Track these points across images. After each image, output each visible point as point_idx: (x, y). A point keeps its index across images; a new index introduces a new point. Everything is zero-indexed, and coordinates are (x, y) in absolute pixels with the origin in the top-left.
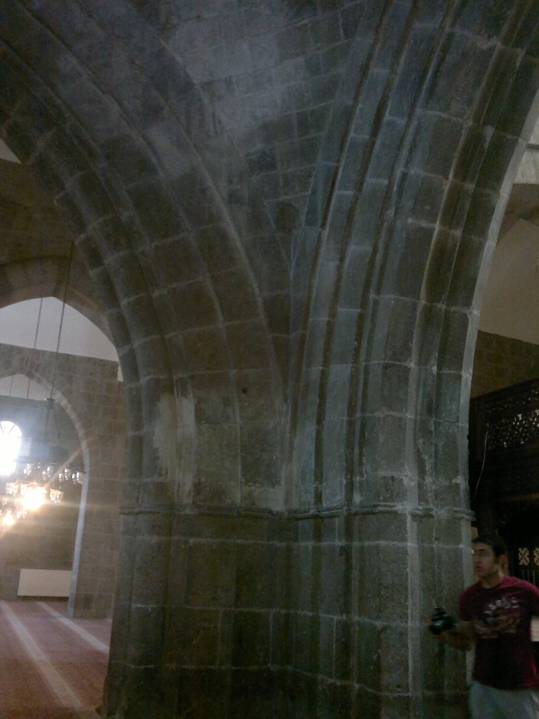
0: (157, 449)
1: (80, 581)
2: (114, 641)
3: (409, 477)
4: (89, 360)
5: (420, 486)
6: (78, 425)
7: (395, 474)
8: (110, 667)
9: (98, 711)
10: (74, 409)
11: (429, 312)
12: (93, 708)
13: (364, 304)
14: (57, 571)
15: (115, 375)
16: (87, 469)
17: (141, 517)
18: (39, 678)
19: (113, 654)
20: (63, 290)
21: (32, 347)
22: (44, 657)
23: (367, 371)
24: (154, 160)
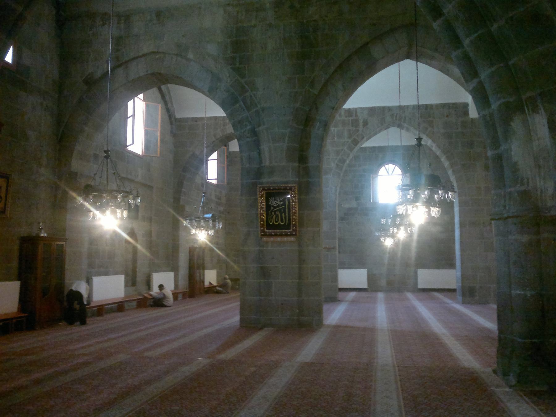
0: (516, 163)
1: (464, 277)
2: (500, 320)
4: (443, 106)
6: (443, 159)
8: (500, 340)
9: (495, 372)
10: (438, 146)
12: (490, 370)
15: (466, 113)
16: (456, 189)
17: (510, 220)
18: (442, 345)
19: (501, 331)
20: (413, 52)
21: (398, 104)
22: (444, 331)
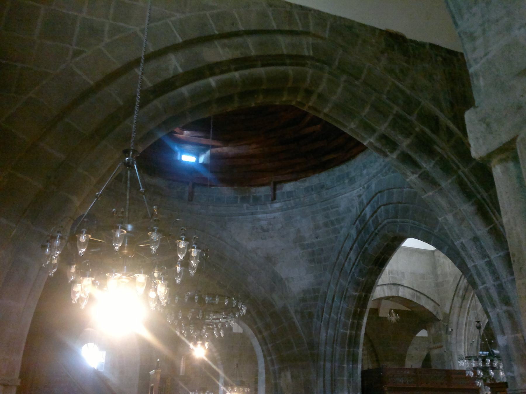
11: (349, 351)
13: (333, 348)
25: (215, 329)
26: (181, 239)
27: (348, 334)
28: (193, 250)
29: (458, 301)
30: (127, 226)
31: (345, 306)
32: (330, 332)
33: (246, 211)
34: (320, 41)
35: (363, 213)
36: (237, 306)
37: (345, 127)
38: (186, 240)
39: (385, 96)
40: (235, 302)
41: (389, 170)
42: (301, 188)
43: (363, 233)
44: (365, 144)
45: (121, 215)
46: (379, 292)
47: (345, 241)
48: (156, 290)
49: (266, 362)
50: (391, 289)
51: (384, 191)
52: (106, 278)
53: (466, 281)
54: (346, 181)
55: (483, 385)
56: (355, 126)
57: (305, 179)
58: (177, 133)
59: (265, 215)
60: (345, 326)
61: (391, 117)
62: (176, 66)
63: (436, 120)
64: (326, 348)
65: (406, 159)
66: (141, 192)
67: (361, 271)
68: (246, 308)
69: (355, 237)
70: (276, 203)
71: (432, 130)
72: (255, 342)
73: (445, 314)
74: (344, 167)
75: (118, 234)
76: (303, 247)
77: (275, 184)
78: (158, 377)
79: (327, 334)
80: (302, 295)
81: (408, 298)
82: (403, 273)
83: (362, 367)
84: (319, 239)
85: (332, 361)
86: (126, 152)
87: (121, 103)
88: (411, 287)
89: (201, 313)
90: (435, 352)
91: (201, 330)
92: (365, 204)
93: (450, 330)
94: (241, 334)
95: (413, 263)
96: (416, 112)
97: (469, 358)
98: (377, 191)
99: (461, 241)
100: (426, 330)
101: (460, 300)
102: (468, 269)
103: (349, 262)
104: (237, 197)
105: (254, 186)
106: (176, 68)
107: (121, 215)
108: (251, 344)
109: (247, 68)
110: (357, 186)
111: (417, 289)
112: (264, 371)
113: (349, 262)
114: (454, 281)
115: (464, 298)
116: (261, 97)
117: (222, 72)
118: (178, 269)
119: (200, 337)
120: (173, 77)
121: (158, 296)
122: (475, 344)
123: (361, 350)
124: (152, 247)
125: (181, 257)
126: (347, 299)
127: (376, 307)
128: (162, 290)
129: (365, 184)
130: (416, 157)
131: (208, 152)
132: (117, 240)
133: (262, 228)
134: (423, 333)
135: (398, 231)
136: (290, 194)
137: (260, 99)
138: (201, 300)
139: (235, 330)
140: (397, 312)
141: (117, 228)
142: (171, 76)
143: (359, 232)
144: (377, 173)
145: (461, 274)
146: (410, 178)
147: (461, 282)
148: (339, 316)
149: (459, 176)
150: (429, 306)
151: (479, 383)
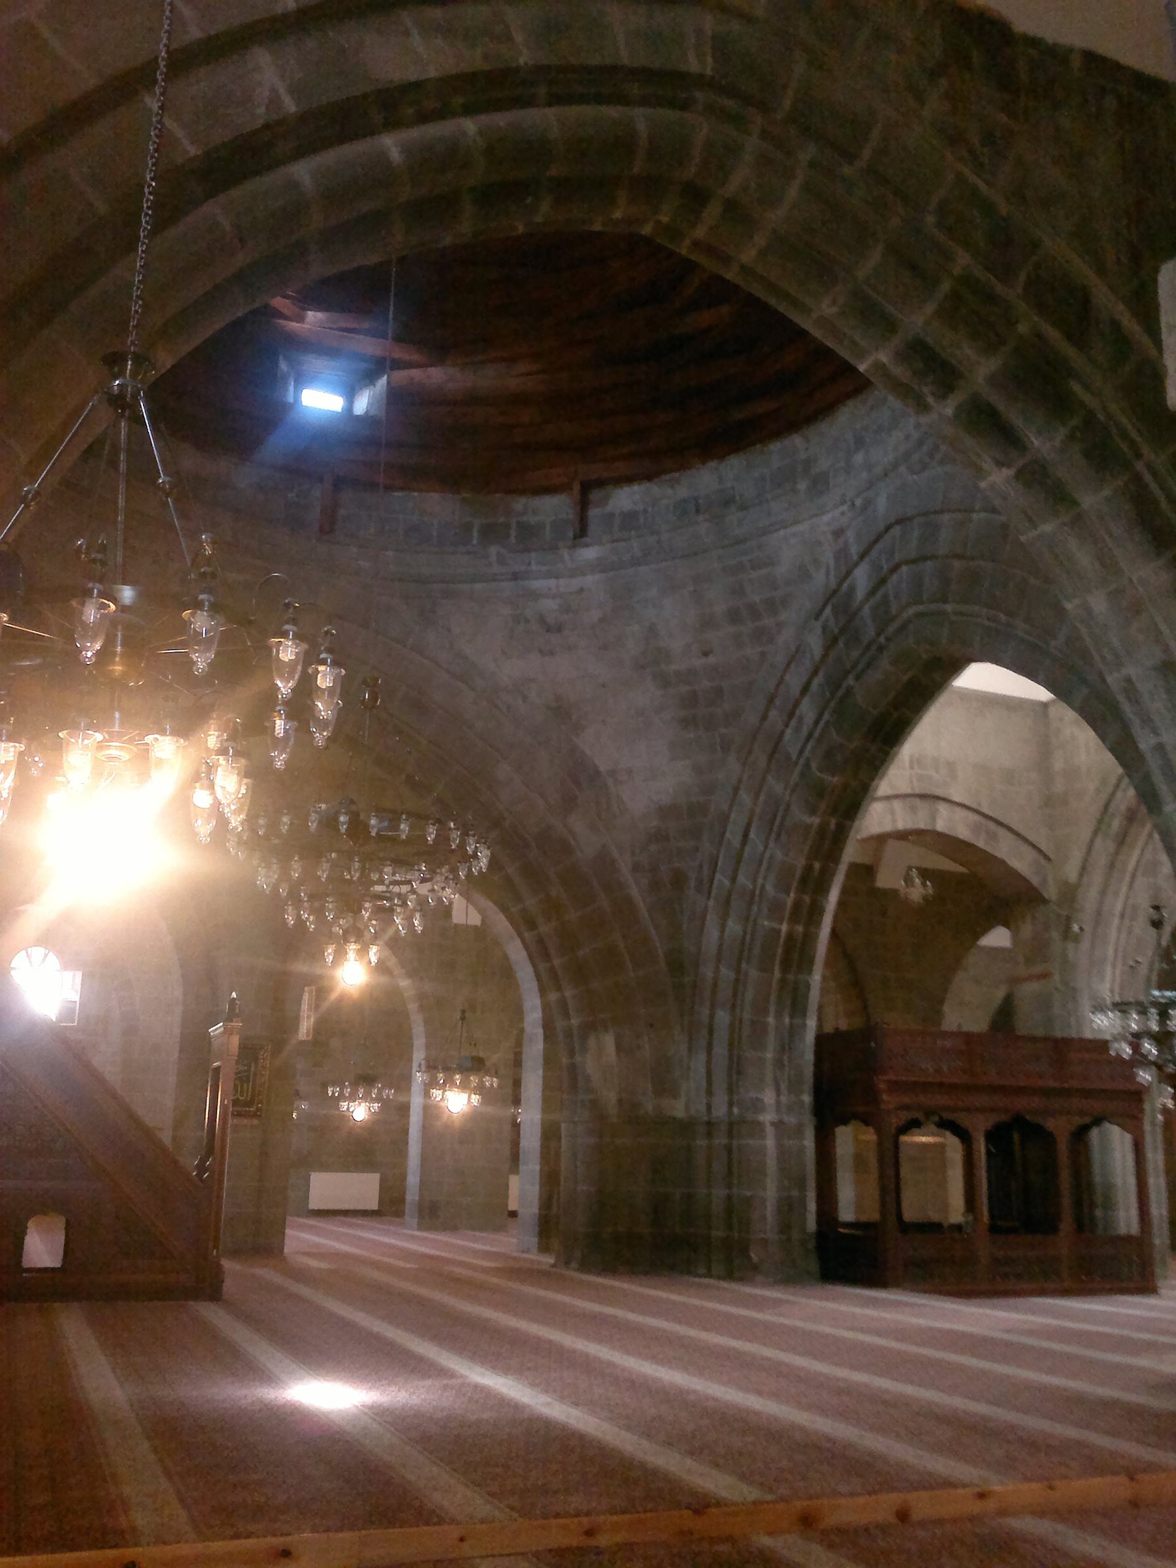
3: (769, 1097)
5: (778, 1103)
7: (759, 1096)
11: (783, 981)
13: (738, 971)
14: (355, 1175)
23: (741, 1021)
24: (573, 842)
25: (399, 910)
26: (285, 635)
27: (783, 934)
28: (321, 668)
29: (1104, 847)
30: (121, 590)
31: (779, 855)
32: (734, 927)
33: (496, 569)
34: (736, 26)
35: (845, 586)
36: (462, 846)
37: (806, 310)
38: (299, 637)
39: (930, 219)
40: (456, 836)
41: (931, 455)
42: (665, 501)
43: (841, 644)
44: (862, 368)
45: (99, 556)
46: (879, 817)
47: (788, 665)
48: (211, 786)
49: (546, 1007)
50: (913, 809)
51: (910, 519)
52: (59, 747)
53: (1131, 792)
54: (802, 486)
55: (1156, 1079)
56: (834, 310)
57: (677, 475)
58: (286, 318)
59: (552, 582)
60: (776, 909)
61: (946, 286)
62: (274, 90)
63: (1085, 300)
64: (717, 971)
65: (984, 420)
66: (158, 488)
67: (829, 754)
68: (488, 853)
69: (817, 657)
70: (587, 545)
71: (1069, 337)
72: (517, 952)
73: (1066, 883)
74: (797, 440)
75: (91, 614)
76: (664, 681)
77: (586, 488)
78: (235, 1041)
79: (722, 932)
80: (655, 823)
81: (961, 837)
82: (951, 766)
83: (820, 1025)
84: (711, 659)
85: (733, 1006)
86: (114, 361)
87: (102, 208)
88: (974, 806)
89: (357, 865)
90: (1029, 989)
91: (357, 911)
92: (855, 557)
93: (1076, 928)
94: (476, 927)
95: (983, 734)
96: (1023, 277)
97: (1122, 1007)
98: (893, 520)
99: (1124, 672)
100: (1008, 928)
101: (1111, 846)
102: (1141, 757)
103: (798, 729)
104: (468, 527)
105: (523, 492)
106: (274, 101)
107: (99, 556)
108: (506, 957)
109: (496, 106)
110: (834, 499)
111: (991, 814)
112: (540, 1031)
113: (798, 729)
114: (1098, 791)
115: (1122, 841)
116: (545, 206)
117: (424, 118)
118: (280, 725)
119: (355, 933)
120: (267, 127)
121: (217, 804)
122: (1143, 970)
123: (816, 978)
124: (194, 656)
125: (285, 687)
126: (784, 837)
127: (867, 860)
128: (230, 784)
129: (858, 496)
130: (1014, 416)
131: (383, 381)
132: (90, 632)
133: (542, 620)
134: (998, 938)
135: (944, 641)
136: (629, 519)
137: (544, 212)
138: (357, 828)
139: (458, 917)
140: (925, 874)
141: (88, 593)
142: (260, 122)
143: (831, 643)
144: (895, 465)
145: (1120, 770)
146: (992, 478)
147: (1119, 794)
148: (760, 881)
149: (1137, 478)
150: (1021, 862)
151: (1145, 1076)
